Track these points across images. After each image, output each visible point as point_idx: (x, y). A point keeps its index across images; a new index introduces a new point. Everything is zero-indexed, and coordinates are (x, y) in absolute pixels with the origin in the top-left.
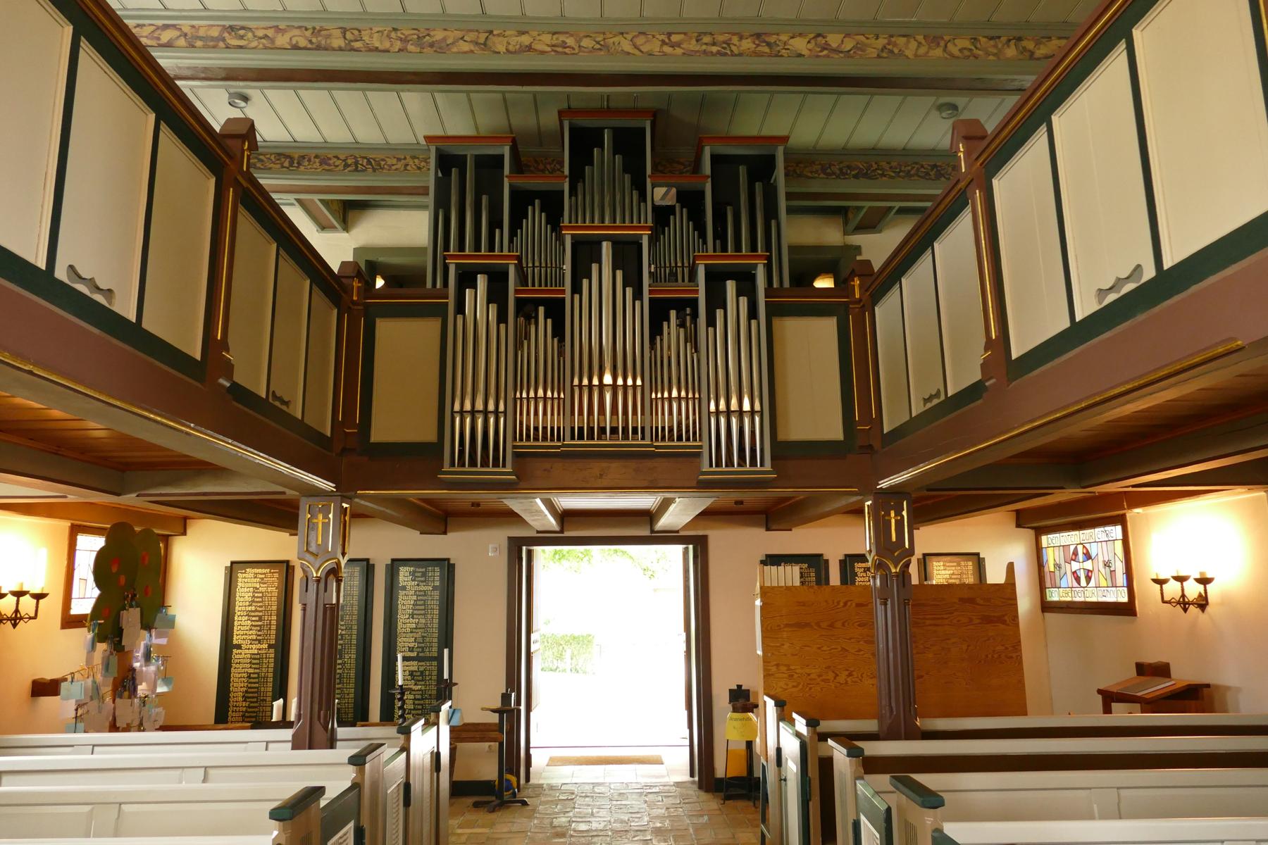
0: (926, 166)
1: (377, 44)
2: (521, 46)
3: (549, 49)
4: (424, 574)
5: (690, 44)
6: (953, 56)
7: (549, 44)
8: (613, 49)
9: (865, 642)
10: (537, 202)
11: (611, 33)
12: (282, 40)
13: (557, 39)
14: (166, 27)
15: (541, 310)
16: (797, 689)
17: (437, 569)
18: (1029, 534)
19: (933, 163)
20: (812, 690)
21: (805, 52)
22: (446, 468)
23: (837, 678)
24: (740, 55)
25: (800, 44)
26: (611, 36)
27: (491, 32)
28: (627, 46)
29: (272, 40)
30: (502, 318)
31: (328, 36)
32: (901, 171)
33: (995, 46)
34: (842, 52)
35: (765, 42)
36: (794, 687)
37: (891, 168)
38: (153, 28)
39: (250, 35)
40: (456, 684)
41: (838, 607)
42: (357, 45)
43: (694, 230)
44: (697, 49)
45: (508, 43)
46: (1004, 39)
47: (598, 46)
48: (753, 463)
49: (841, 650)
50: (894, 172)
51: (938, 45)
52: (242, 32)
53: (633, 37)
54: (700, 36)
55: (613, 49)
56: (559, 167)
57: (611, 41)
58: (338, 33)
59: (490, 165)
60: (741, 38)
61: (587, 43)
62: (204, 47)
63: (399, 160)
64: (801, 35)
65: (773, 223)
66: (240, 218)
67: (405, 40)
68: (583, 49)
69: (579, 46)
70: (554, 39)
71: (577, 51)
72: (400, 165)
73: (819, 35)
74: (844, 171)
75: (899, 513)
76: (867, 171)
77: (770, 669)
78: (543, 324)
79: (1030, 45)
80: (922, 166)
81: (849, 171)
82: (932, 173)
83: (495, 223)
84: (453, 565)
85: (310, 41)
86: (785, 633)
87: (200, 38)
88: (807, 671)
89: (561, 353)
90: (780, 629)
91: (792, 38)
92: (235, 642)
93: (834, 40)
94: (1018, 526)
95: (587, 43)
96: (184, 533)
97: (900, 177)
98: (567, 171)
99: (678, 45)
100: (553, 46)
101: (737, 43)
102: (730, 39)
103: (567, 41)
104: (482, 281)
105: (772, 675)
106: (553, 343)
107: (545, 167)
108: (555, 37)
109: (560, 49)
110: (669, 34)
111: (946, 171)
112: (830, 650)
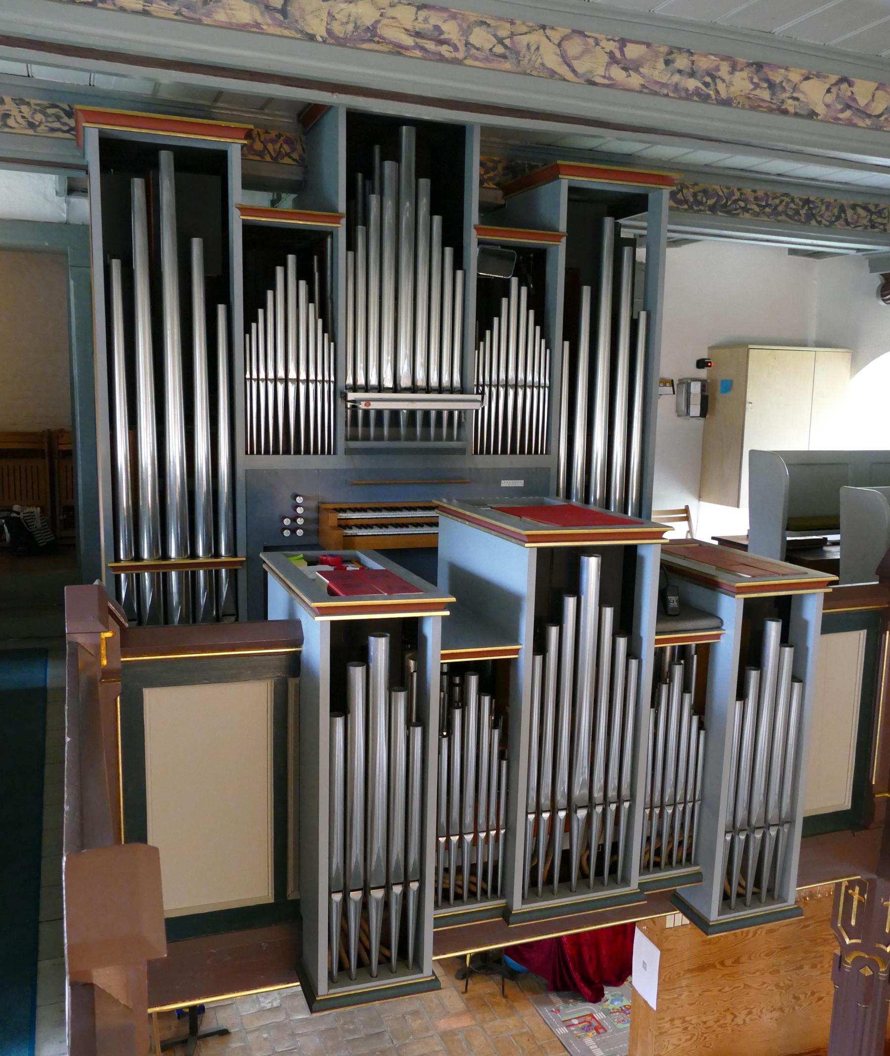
0: (797, 200)
2: (356, 27)
3: (409, 41)
5: (654, 68)
7: (408, 27)
8: (526, 60)
9: (771, 973)
10: (291, 259)
11: (524, 23)
13: (426, 20)
16: (692, 1041)
19: (806, 197)
20: (707, 1040)
21: (820, 109)
23: (735, 1019)
24: (727, 103)
26: (524, 29)
28: (552, 60)
32: (767, 205)
34: (869, 116)
35: (767, 80)
36: (687, 1040)
37: (756, 198)
41: (747, 938)
43: (528, 309)
44: (664, 81)
45: (332, 17)
47: (499, 49)
49: (744, 988)
50: (759, 206)
53: (562, 39)
54: (671, 53)
55: (526, 60)
56: (288, 150)
57: (524, 40)
60: (734, 69)
61: (480, 38)
64: (818, 76)
65: (221, 309)
68: (474, 51)
69: (467, 44)
70: (420, 19)
71: (460, 55)
73: (844, 80)
74: (699, 198)
76: (727, 202)
77: (664, 1027)
80: (793, 201)
81: (704, 200)
82: (803, 212)
86: (685, 980)
88: (704, 1019)
90: (679, 977)
91: (807, 78)
95: (480, 38)
97: (764, 213)
100: (418, 34)
101: (727, 77)
102: (717, 69)
103: (445, 27)
104: (379, 648)
105: (665, 1032)
106: (491, 738)
107: (265, 147)
108: (423, 14)
109: (430, 46)
110: (623, 43)
111: (818, 210)
112: (732, 990)
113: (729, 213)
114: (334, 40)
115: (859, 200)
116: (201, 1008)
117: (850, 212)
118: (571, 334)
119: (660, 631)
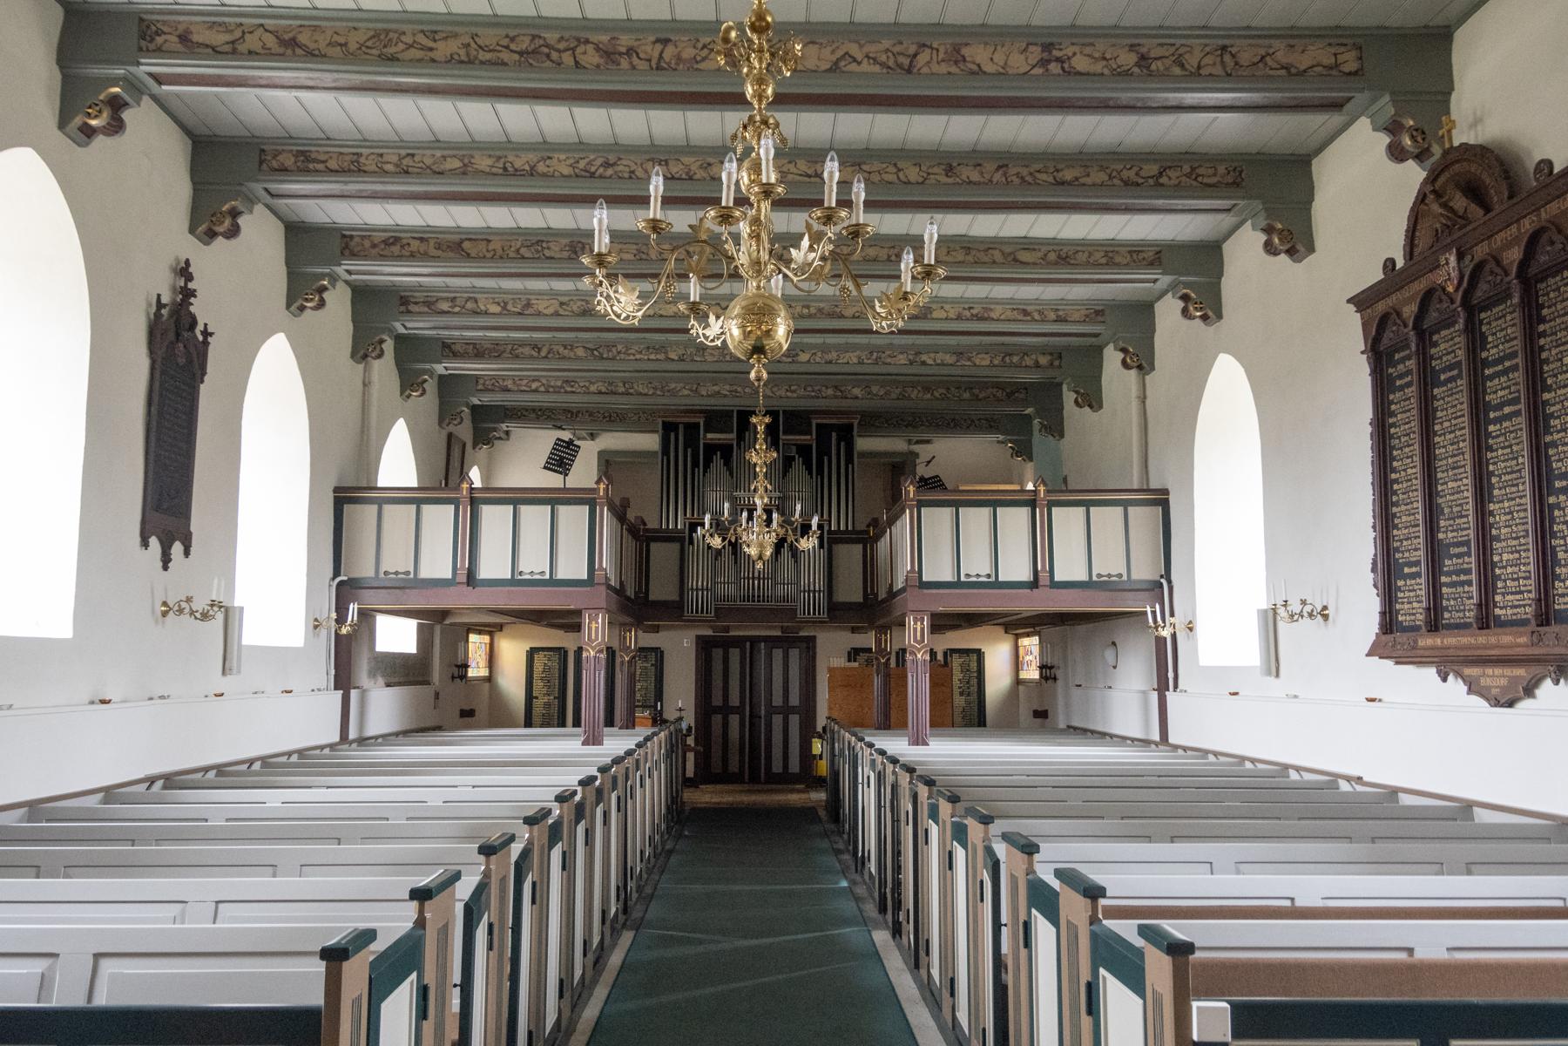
4: (646, 657)
12: (593, 388)
14: (534, 381)
18: (1010, 638)
22: (686, 614)
25: (857, 391)
40: (1362, 353)
42: (631, 391)
48: (819, 614)
59: (692, 428)
60: (827, 388)
62: (555, 392)
65: (850, 466)
75: (886, 635)
79: (976, 391)
83: (695, 464)
93: (875, 389)
94: (1006, 632)
99: (794, 391)
113: (914, 427)
114: (708, 396)
116: (100, 803)
117: (977, 422)
118: (820, 472)
119: (230, 614)
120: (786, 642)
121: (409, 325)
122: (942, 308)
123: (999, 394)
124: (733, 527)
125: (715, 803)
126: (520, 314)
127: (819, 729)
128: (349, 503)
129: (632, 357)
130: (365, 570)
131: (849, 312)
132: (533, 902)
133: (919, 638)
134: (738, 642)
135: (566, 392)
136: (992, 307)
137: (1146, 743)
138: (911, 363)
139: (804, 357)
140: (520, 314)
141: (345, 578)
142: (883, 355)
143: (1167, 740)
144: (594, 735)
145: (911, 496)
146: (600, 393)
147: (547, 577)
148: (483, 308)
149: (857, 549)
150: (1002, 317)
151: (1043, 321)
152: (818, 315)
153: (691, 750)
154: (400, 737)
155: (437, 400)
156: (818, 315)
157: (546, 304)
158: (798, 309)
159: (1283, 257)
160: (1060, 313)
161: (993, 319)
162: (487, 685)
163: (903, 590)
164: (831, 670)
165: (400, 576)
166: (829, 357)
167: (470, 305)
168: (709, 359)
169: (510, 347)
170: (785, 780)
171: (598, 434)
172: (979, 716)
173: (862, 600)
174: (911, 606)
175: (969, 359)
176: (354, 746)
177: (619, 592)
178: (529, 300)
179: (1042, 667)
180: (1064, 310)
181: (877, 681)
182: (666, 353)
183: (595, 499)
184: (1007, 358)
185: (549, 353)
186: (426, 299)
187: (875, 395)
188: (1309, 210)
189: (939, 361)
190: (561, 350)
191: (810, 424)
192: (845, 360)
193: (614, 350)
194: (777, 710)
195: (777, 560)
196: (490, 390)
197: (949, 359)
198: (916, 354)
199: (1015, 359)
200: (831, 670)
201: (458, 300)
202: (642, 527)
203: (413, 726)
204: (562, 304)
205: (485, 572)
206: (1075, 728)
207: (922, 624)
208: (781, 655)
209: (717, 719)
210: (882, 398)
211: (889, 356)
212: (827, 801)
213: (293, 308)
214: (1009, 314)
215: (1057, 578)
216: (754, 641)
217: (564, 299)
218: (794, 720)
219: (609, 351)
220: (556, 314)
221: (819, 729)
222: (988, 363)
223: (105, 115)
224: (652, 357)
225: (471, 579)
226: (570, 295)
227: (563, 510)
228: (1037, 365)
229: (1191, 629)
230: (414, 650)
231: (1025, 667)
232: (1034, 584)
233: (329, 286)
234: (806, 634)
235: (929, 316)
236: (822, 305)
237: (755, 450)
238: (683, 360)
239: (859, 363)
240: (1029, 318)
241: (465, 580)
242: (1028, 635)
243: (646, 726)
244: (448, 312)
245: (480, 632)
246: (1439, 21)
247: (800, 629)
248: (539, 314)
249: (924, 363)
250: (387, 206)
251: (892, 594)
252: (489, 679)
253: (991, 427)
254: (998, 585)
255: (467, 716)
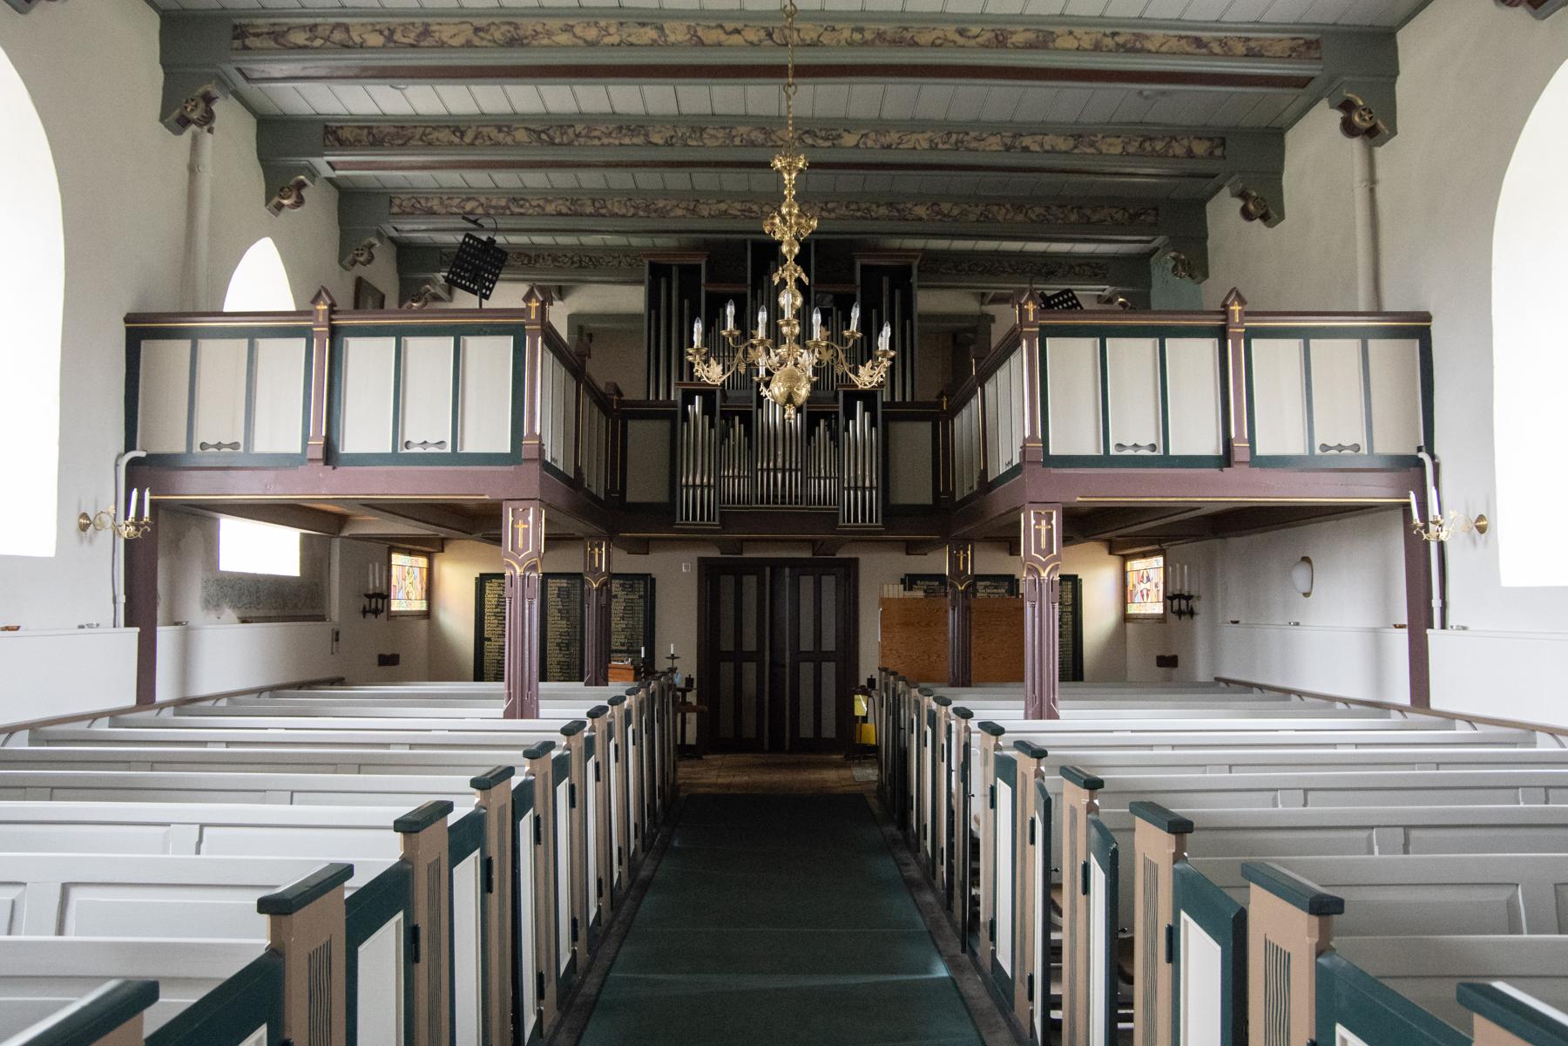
1: (616, 210)
3: (739, 213)
4: (631, 586)
6: (1030, 219)
12: (550, 209)
14: (469, 199)
15: (737, 418)
17: (641, 582)
21: (925, 216)
22: (678, 521)
25: (921, 211)
27: (698, 201)
29: (543, 209)
30: (712, 425)
31: (581, 205)
33: (1063, 213)
38: (459, 200)
39: (527, 205)
42: (603, 211)
46: (1069, 207)
48: (871, 521)
51: (1021, 212)
52: (522, 202)
58: (589, 202)
59: (690, 272)
60: (878, 206)
63: (615, 258)
66: (545, 354)
67: (636, 208)
72: (615, 262)
75: (965, 552)
78: (738, 427)
79: (1088, 212)
80: (1035, 265)
84: (654, 579)
85: (570, 209)
87: (495, 207)
89: (750, 447)
91: (916, 205)
92: (486, 636)
94: (1110, 553)
96: (443, 551)
98: (749, 282)
99: (833, 210)
100: (744, 211)
109: (747, 214)
110: (826, 203)
115: (1083, 261)
117: (1077, 269)
120: (817, 567)
121: (399, 227)
122: (1071, 33)
123: (1119, 216)
124: (742, 348)
125: (721, 786)
126: (412, 46)
127: (863, 682)
128: (149, 337)
129: (596, 142)
130: (173, 443)
131: (925, 38)
132: (598, 779)
133: (1043, 546)
134: (756, 566)
135: (512, 214)
136: (1147, 32)
137: (1380, 707)
138: (1008, 149)
139: (849, 140)
140: (412, 46)
141: (143, 454)
142: (966, 138)
143: (1428, 704)
144: (522, 700)
145: (1031, 318)
146: (560, 214)
147: (448, 449)
148: (357, 40)
149: (925, 428)
150: (1164, 49)
151: (1226, 55)
152: (877, 42)
153: (693, 709)
154: (265, 697)
155: (397, 275)
156: (877, 42)
157: (454, 30)
158: (846, 34)
159: (1258, 222)
160: (1252, 44)
161: (1149, 51)
162: (423, 623)
163: (1015, 471)
164: (884, 602)
165: (224, 450)
166: (886, 140)
167: (338, 36)
168: (709, 142)
169: (420, 130)
170: (815, 748)
171: (571, 287)
172: (1074, 666)
173: (931, 502)
174: (1031, 494)
175: (1092, 144)
176: (167, 713)
177: (574, 483)
178: (427, 25)
179: (1169, 598)
180: (1257, 39)
181: (953, 618)
182: (646, 135)
183: (523, 325)
184: (1147, 144)
185: (476, 138)
186: (272, 29)
187: (945, 216)
188: (1394, 83)
189: (1047, 147)
190: (494, 133)
191: (852, 265)
192: (910, 145)
193: (570, 131)
194: (807, 657)
195: (809, 443)
196: (409, 214)
197: (1062, 144)
198: (1014, 137)
199: (1159, 146)
200: (884, 602)
201: (320, 28)
202: (615, 397)
203: (293, 679)
204: (477, 30)
205: (353, 442)
206: (1228, 682)
207: (1049, 522)
208: (811, 585)
209: (727, 669)
210: (955, 219)
211: (975, 139)
212: (881, 787)
213: (346, 262)
214: (1174, 44)
215: (1261, 450)
216: (777, 564)
217: (482, 22)
218: (829, 669)
219: (562, 134)
220: (469, 45)
221: (863, 682)
222: (1119, 150)
223: (294, 195)
224: (627, 141)
225: (330, 454)
226: (491, 15)
227: (473, 344)
228: (1190, 154)
229: (1482, 530)
230: (297, 574)
231: (1138, 598)
232: (1226, 459)
233: (307, 182)
234: (846, 556)
235: (1051, 45)
236: (882, 27)
237: (780, 213)
238: (672, 145)
239: (931, 148)
240: (1204, 51)
241: (319, 454)
242: (1144, 555)
243: (626, 680)
244: (305, 47)
245: (410, 553)
246: (1276, 124)
247: (839, 545)
248: (442, 45)
249: (1026, 149)
250: (369, 88)
251: (986, 486)
252: (428, 614)
253: (1096, 275)
254: (1168, 461)
255: (389, 665)
